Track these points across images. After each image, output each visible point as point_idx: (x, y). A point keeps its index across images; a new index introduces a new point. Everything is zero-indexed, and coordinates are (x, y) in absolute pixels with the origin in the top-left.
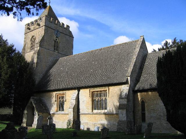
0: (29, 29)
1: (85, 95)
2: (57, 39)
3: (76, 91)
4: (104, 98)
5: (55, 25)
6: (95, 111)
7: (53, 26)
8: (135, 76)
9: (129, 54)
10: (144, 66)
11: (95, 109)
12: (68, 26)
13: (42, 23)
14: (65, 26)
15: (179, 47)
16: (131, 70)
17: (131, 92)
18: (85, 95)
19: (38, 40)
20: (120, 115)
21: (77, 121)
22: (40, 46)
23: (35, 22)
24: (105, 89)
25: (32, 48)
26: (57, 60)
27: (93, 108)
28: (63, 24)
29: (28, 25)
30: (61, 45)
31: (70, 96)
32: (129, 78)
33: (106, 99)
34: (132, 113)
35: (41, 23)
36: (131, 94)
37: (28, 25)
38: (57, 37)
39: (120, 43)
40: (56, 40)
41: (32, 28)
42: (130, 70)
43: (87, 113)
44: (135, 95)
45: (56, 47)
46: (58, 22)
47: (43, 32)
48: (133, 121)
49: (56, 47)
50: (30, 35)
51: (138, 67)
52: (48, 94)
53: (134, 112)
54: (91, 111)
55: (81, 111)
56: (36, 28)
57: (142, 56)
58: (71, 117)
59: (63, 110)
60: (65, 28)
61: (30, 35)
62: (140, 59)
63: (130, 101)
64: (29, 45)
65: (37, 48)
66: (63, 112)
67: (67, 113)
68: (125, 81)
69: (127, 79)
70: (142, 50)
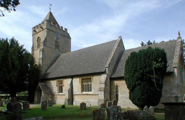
0: (35, 31)
1: (77, 82)
2: (58, 40)
3: (70, 80)
4: (90, 83)
5: (55, 28)
6: (84, 93)
7: (53, 29)
8: (112, 67)
9: (110, 51)
10: (173, 58)
11: (84, 91)
12: (66, 29)
13: (44, 27)
14: (64, 29)
15: (150, 48)
16: (109, 63)
17: (109, 79)
18: (77, 82)
19: (42, 40)
20: (100, 95)
21: (71, 100)
22: (44, 45)
23: (39, 26)
24: (89, 77)
25: (39, 46)
26: (60, 56)
27: (83, 90)
28: (62, 27)
29: (34, 28)
30: (61, 45)
31: (67, 82)
32: (107, 69)
33: (91, 84)
34: (109, 94)
35: (43, 27)
36: (109, 81)
37: (34, 28)
38: (57, 38)
39: (127, 49)
40: (57, 40)
41: (37, 30)
42: (108, 63)
43: (78, 94)
44: (111, 82)
45: (57, 46)
46: (58, 25)
47: (46, 34)
48: (110, 99)
49: (57, 46)
50: (36, 36)
51: (115, 61)
52: (49, 81)
53: (110, 93)
54: (80, 92)
55: (74, 93)
56: (40, 31)
57: (119, 52)
58: (67, 97)
59: (62, 92)
60: (63, 31)
61: (36, 36)
62: (117, 55)
63: (107, 85)
64: (36, 44)
65: (42, 47)
66: (62, 94)
67: (65, 94)
68: (104, 71)
69: (106, 69)
70: (119, 47)
